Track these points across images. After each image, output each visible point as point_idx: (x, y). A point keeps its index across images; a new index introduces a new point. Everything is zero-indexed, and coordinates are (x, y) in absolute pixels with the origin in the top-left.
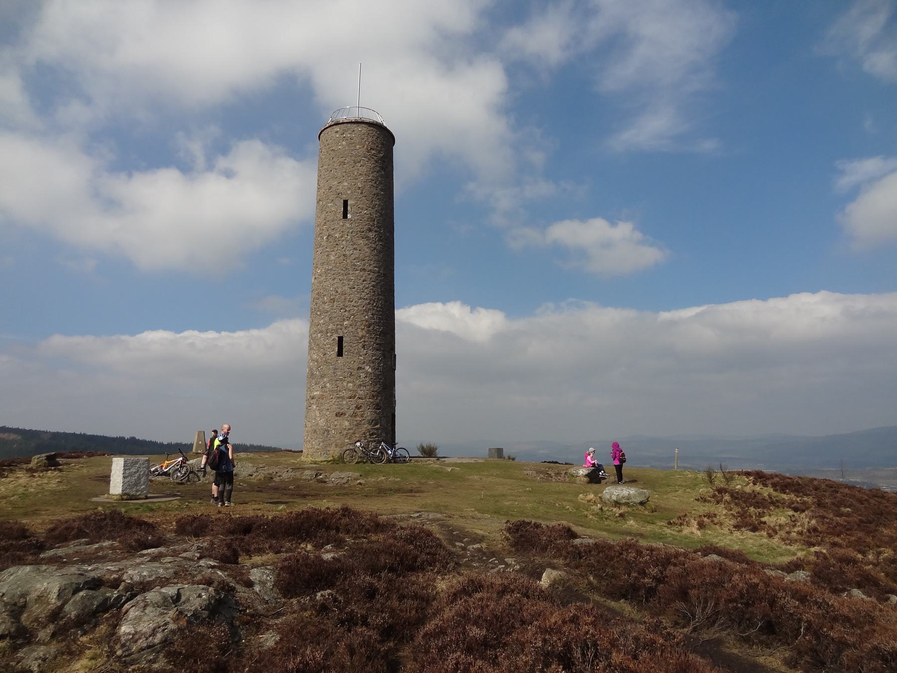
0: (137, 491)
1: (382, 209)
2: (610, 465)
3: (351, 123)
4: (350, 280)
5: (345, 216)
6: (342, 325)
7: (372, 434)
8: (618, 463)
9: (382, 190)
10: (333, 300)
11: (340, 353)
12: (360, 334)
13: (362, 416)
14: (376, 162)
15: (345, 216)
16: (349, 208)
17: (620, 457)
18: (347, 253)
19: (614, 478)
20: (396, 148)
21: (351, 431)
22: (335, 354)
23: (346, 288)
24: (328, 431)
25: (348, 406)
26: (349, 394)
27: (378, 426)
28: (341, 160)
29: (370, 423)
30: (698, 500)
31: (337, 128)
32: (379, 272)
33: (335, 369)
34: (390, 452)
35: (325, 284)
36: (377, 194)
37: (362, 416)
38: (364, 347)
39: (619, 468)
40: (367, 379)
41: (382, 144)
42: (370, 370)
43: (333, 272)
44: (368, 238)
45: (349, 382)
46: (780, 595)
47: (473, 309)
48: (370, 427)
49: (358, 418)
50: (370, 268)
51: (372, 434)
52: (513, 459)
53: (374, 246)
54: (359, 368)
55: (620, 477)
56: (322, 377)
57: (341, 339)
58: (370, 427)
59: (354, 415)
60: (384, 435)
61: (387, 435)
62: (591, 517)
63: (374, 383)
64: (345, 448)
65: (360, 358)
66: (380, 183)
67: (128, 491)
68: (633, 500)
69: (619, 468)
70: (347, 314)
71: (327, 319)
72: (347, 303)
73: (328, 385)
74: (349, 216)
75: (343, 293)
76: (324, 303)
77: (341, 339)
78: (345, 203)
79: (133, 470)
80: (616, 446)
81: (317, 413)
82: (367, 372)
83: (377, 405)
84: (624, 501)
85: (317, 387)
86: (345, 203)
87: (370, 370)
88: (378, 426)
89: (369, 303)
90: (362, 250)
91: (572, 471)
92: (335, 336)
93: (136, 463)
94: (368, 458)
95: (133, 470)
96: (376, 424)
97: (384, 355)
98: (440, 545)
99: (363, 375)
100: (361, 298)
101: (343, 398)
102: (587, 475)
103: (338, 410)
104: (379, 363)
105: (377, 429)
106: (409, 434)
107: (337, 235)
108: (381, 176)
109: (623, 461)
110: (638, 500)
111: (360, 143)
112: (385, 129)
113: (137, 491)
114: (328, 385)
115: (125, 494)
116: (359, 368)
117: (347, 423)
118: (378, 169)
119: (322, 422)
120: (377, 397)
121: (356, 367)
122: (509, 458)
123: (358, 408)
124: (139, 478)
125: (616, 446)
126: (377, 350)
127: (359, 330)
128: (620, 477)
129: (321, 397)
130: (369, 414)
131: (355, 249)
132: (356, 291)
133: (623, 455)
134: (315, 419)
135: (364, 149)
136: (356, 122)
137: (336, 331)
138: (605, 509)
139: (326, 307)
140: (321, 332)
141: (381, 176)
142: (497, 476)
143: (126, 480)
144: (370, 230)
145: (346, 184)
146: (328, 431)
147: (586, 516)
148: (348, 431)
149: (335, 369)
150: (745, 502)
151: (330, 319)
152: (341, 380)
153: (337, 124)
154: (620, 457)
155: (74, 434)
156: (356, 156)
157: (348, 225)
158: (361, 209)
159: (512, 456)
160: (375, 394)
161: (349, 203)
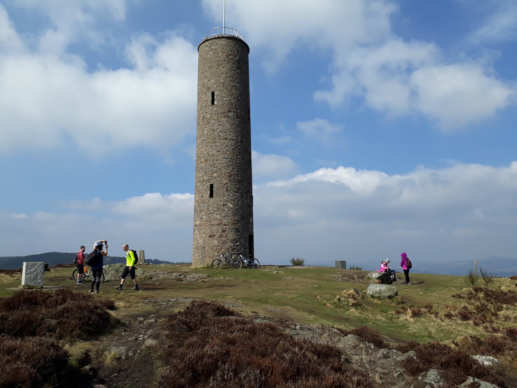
0: (36, 283)
1: (238, 96)
2: (400, 270)
3: (215, 38)
4: (217, 146)
5: (213, 103)
6: (212, 177)
7: (233, 249)
8: (406, 269)
9: (238, 83)
11: (211, 195)
12: (225, 182)
13: (226, 237)
14: (233, 63)
15: (213, 103)
16: (215, 97)
17: (406, 263)
18: (215, 128)
19: (403, 280)
20: (250, 55)
21: (219, 247)
23: (215, 152)
25: (217, 230)
26: (217, 222)
27: (238, 244)
28: (210, 64)
29: (232, 242)
30: (453, 296)
31: (207, 44)
32: (237, 140)
33: (209, 206)
34: (245, 261)
36: (235, 86)
37: (226, 237)
38: (227, 190)
39: (406, 272)
40: (230, 212)
41: (238, 51)
42: (231, 206)
43: (206, 142)
44: (228, 117)
47: (357, 170)
48: (232, 244)
49: (224, 239)
50: (231, 137)
51: (233, 249)
52: (361, 269)
53: (232, 122)
54: (224, 205)
55: (408, 280)
56: (201, 211)
57: (212, 186)
58: (232, 244)
59: (221, 236)
60: (242, 250)
61: (245, 249)
62: (329, 305)
63: (235, 214)
64: (215, 259)
65: (225, 200)
66: (237, 78)
67: (29, 283)
68: (383, 294)
69: (406, 272)
70: (215, 169)
71: (203, 173)
72: (215, 162)
73: (204, 217)
74: (215, 103)
75: (213, 155)
76: (202, 162)
77: (212, 186)
78: (213, 94)
79: (32, 270)
80: (404, 256)
83: (237, 229)
84: (377, 295)
85: (198, 219)
86: (213, 94)
87: (231, 206)
88: (238, 244)
89: (230, 161)
90: (224, 126)
91: (369, 275)
92: (208, 184)
93: (35, 265)
94: (231, 265)
95: (32, 270)
96: (237, 242)
97: (242, 196)
99: (226, 210)
100: (224, 158)
101: (213, 225)
102: (379, 278)
103: (210, 233)
104: (238, 201)
105: (237, 246)
106: (268, 249)
107: (208, 116)
108: (237, 73)
109: (410, 266)
110: (388, 294)
112: (240, 40)
113: (36, 283)
114: (204, 217)
115: (27, 285)
116: (224, 205)
117: (216, 242)
118: (235, 68)
119: (201, 241)
120: (237, 224)
121: (222, 204)
122: (357, 269)
123: (224, 231)
124: (37, 275)
125: (404, 256)
126: (237, 192)
128: (408, 280)
129: (201, 225)
130: (231, 235)
131: (220, 125)
132: (222, 153)
133: (410, 262)
135: (224, 56)
136: (219, 38)
138: (343, 299)
140: (200, 182)
141: (237, 73)
142: (309, 278)
143: (27, 276)
144: (230, 111)
145: (213, 81)
146: (204, 247)
147: (325, 305)
148: (217, 248)
149: (209, 206)
150: (495, 299)
151: (205, 173)
152: (212, 213)
153: (206, 41)
154: (406, 263)
155: (67, 253)
156: (219, 61)
158: (224, 98)
159: (359, 267)
160: (235, 222)
161: (215, 93)
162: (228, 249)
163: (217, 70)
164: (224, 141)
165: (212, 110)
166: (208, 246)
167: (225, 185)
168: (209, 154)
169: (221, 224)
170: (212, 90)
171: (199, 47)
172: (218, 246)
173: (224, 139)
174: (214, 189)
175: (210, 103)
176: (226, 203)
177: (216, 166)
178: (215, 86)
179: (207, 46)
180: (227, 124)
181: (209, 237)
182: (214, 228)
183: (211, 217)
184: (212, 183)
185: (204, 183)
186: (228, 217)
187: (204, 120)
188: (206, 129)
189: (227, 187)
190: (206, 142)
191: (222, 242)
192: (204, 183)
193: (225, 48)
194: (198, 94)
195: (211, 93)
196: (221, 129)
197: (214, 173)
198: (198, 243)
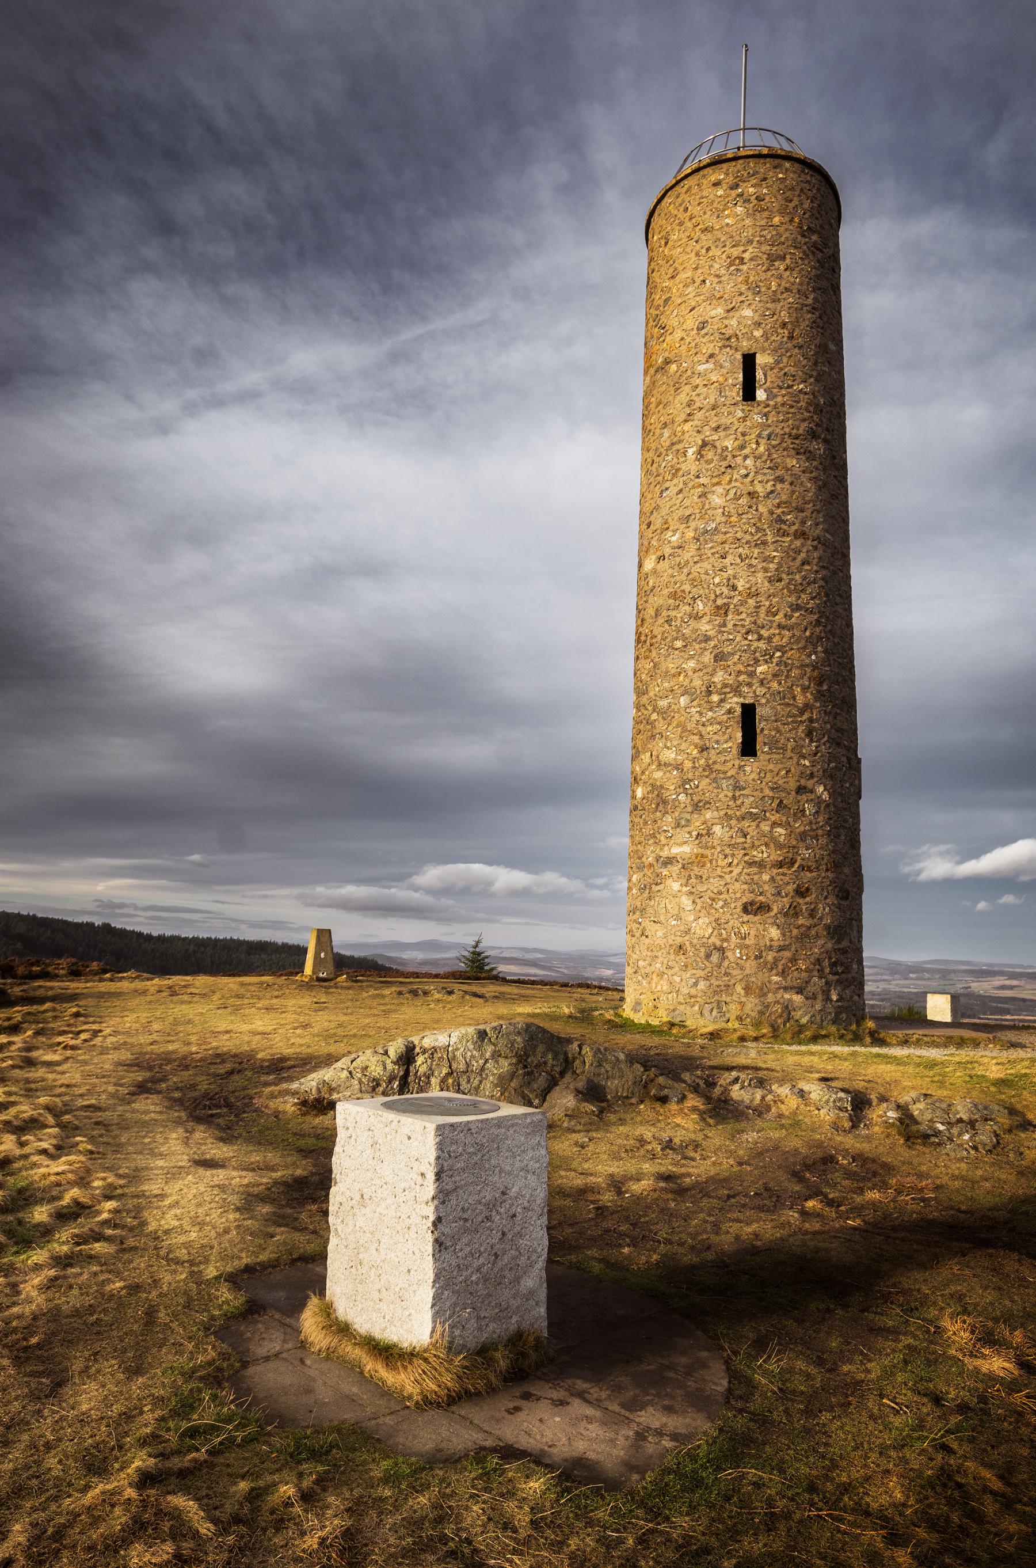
4: (767, 559)
6: (752, 674)
10: (722, 610)
11: (748, 748)
12: (800, 700)
15: (749, 393)
16: (759, 375)
18: (759, 488)
21: (787, 954)
22: (735, 751)
24: (722, 950)
26: (776, 855)
28: (736, 252)
35: (697, 568)
38: (809, 733)
43: (720, 538)
44: (809, 455)
45: (775, 824)
46: (622, 1057)
57: (748, 713)
59: (793, 912)
70: (762, 645)
71: (708, 658)
74: (761, 395)
76: (697, 617)
77: (748, 713)
78: (749, 362)
81: (686, 902)
82: (818, 802)
86: (749, 362)
87: (826, 796)
92: (734, 702)
98: (75, 973)
100: (798, 608)
101: (761, 865)
103: (747, 898)
107: (729, 443)
111: (782, 212)
114: (717, 829)
116: (800, 790)
117: (774, 933)
121: (793, 785)
123: (801, 892)
127: (798, 690)
134: (678, 918)
137: (737, 691)
139: (705, 627)
145: (748, 312)
146: (722, 950)
152: (753, 817)
157: (758, 418)
161: (761, 360)
162: (818, 961)
163: (763, 276)
164: (798, 543)
165: (744, 419)
166: (741, 947)
167: (802, 712)
168: (734, 588)
169: (792, 862)
170: (745, 345)
171: (652, 214)
172: (781, 949)
173: (796, 536)
174: (760, 725)
175: (736, 393)
176: (810, 784)
177: (765, 633)
178: (758, 333)
179: (717, 184)
180: (804, 478)
181: (745, 910)
182: (766, 877)
183: (752, 831)
184: (749, 701)
185: (715, 698)
186: (816, 838)
187: (710, 455)
188: (719, 490)
189: (811, 720)
190: (720, 538)
191: (795, 932)
192: (715, 698)
193: (796, 202)
194: (439, 1244)
195: (739, 356)
196: (784, 497)
197: (757, 661)
198: (687, 932)
